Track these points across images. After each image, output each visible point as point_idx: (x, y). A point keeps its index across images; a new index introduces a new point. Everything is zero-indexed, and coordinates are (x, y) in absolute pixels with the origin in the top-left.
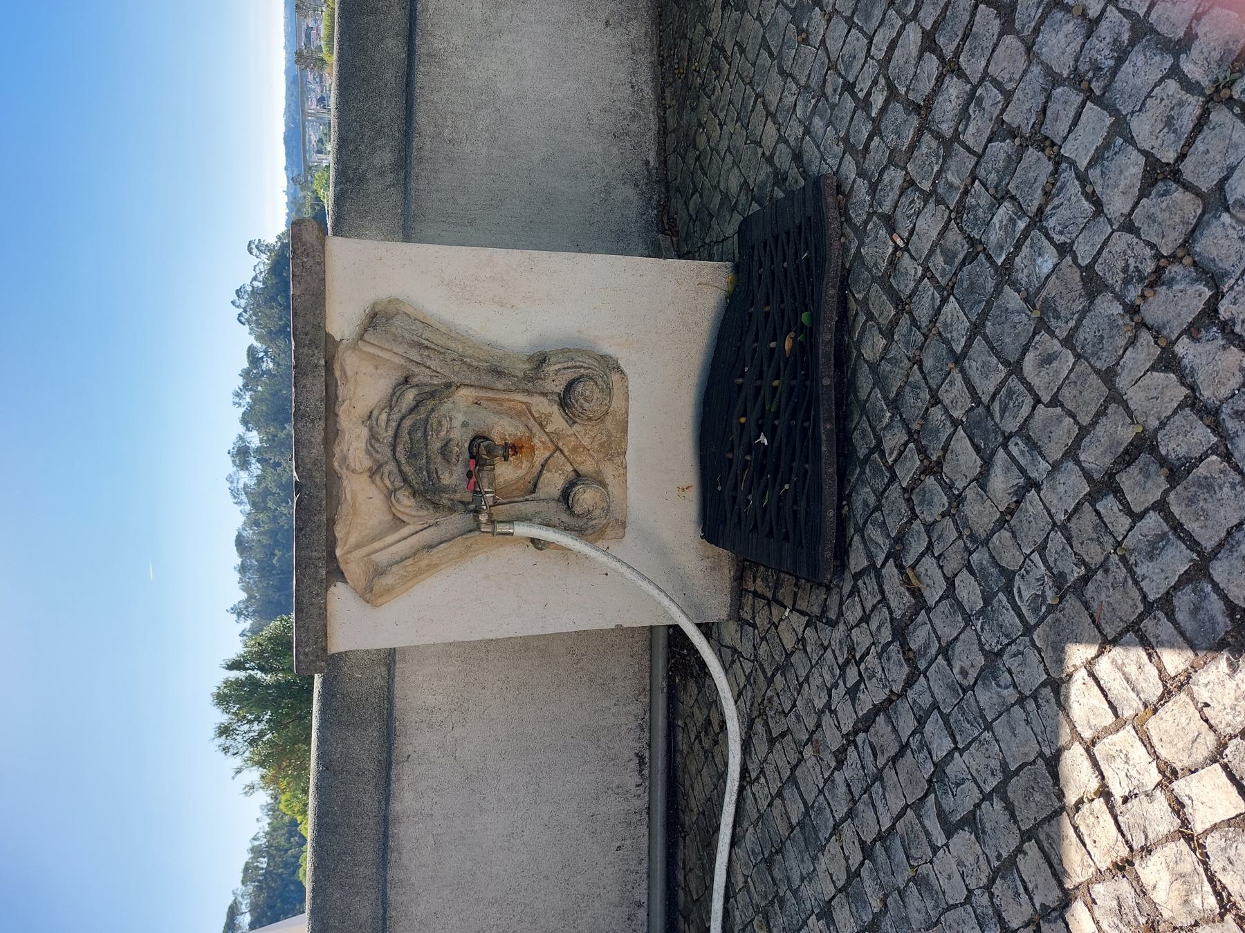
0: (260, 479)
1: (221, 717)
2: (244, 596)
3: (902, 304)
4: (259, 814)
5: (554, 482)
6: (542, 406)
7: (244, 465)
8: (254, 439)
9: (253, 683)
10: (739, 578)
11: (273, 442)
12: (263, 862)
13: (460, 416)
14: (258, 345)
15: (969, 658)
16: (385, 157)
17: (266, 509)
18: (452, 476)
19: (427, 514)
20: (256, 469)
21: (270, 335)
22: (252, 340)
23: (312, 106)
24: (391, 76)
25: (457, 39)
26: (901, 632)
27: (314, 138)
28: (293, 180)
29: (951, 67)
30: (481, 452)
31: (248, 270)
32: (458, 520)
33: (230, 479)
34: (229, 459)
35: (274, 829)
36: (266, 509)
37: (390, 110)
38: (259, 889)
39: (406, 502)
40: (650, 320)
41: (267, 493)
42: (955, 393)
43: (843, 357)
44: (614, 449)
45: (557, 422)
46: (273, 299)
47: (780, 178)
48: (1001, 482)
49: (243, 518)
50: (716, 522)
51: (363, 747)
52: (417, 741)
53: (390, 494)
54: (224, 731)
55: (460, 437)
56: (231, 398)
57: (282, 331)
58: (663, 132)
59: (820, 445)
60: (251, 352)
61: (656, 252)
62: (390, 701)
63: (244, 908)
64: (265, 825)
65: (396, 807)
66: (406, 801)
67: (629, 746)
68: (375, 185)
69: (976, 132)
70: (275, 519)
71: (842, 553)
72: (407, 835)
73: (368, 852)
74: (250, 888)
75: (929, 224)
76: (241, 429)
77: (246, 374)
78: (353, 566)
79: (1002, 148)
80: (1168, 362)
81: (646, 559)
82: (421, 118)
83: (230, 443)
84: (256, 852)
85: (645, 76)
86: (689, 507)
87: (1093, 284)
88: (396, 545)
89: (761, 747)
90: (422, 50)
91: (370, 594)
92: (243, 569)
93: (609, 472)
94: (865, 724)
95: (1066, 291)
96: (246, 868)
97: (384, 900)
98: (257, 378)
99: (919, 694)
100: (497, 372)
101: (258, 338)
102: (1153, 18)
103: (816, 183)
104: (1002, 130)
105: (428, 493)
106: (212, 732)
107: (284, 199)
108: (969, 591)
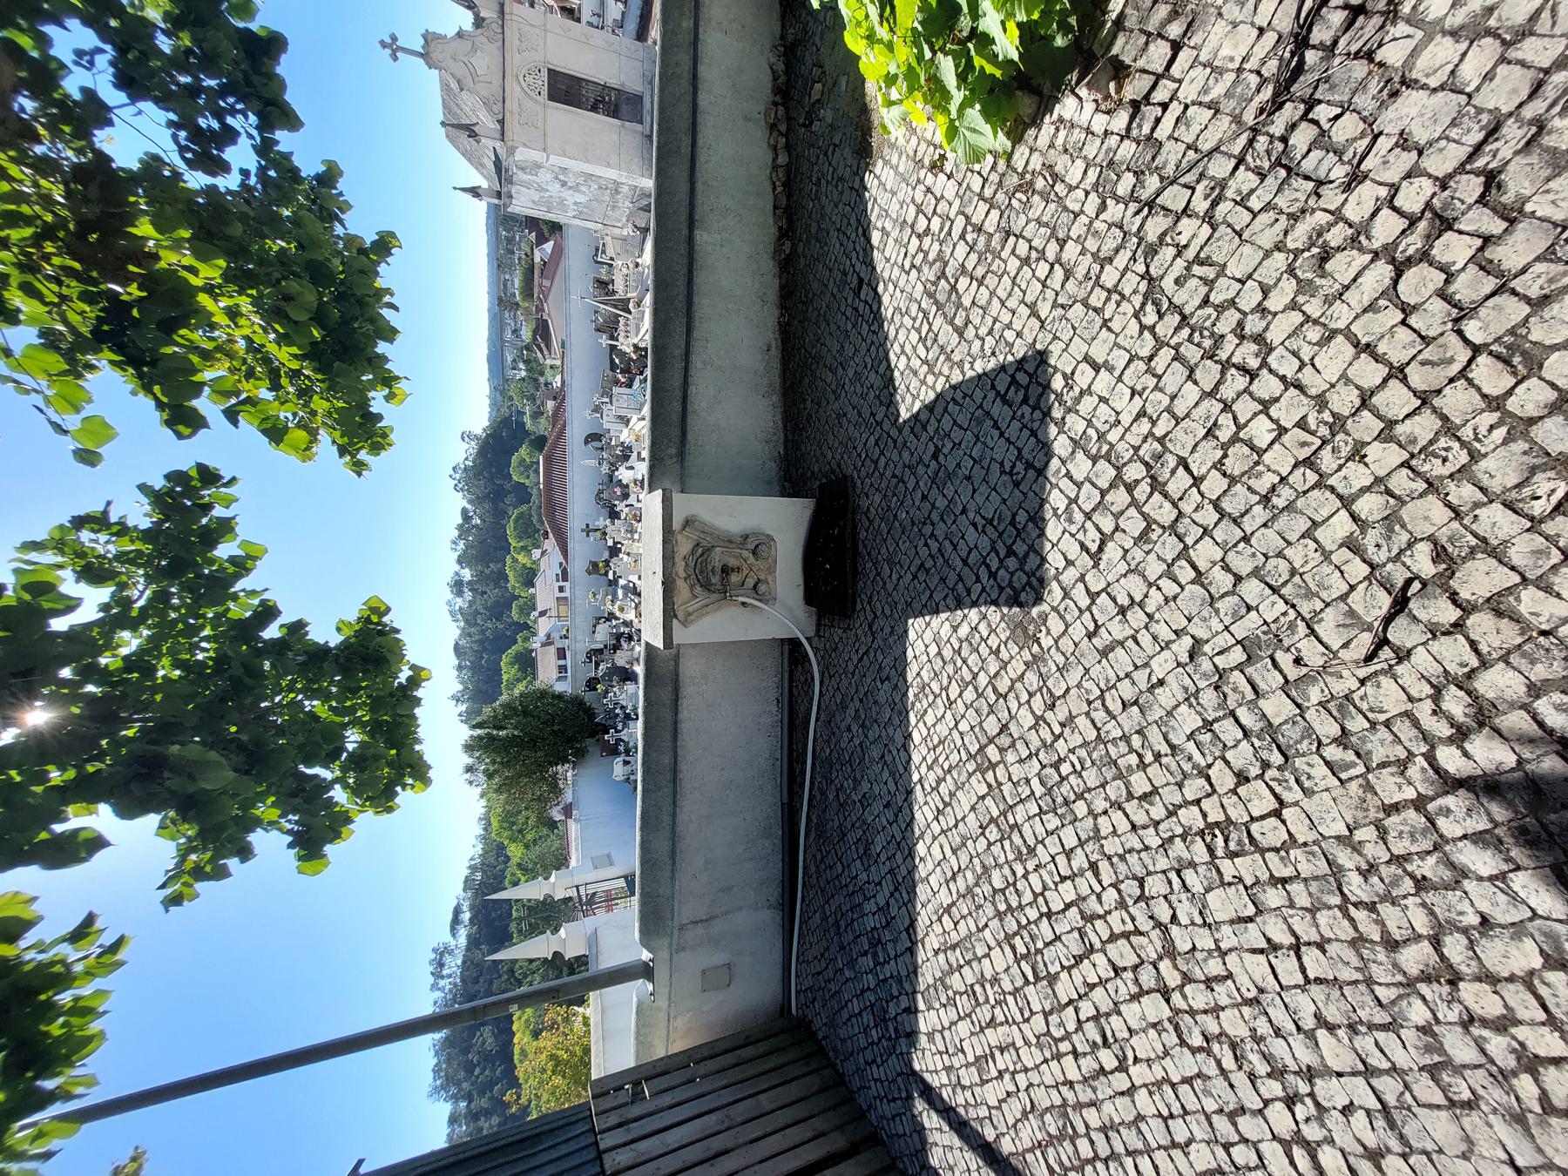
0: (471, 603)
1: (467, 760)
2: (461, 687)
3: (871, 522)
4: (474, 842)
5: (750, 582)
6: (746, 554)
7: (460, 593)
8: (467, 574)
9: (491, 738)
10: (819, 620)
11: (480, 577)
12: (478, 876)
13: (718, 558)
14: (469, 507)
15: (887, 630)
16: (673, 451)
17: (476, 624)
18: (715, 580)
19: (706, 594)
20: (468, 595)
21: (477, 501)
22: (465, 504)
23: (509, 335)
24: (675, 418)
25: (704, 404)
26: (870, 627)
27: (509, 359)
28: (495, 389)
29: (882, 453)
30: (726, 570)
31: (461, 453)
32: (716, 596)
33: (449, 603)
34: (448, 589)
35: (485, 853)
36: (476, 624)
37: (675, 432)
38: (476, 894)
39: (698, 589)
40: (782, 521)
41: (477, 613)
42: (884, 551)
43: (855, 536)
44: (772, 570)
45: (752, 559)
46: (480, 473)
47: (833, 472)
48: (894, 577)
49: (458, 632)
50: (810, 597)
51: (665, 695)
52: (688, 690)
53: (692, 587)
54: (469, 769)
55: (718, 566)
56: (449, 545)
57: (487, 496)
58: (786, 441)
59: (21, 214)
60: (464, 512)
61: (784, 493)
62: (677, 675)
63: (465, 908)
64: (479, 849)
65: (680, 716)
66: (684, 714)
67: (773, 695)
68: (668, 462)
69: (888, 473)
70: (483, 632)
71: (854, 605)
72: (685, 727)
73: (668, 736)
74: (469, 894)
75: (877, 498)
76: (457, 567)
77: (460, 527)
78: (680, 614)
79: (894, 480)
80: (926, 545)
81: (783, 613)
82: (689, 437)
83: (448, 577)
84: (473, 868)
85: (779, 418)
86: (800, 592)
87: (913, 523)
88: (694, 605)
89: (826, 682)
90: (690, 409)
91: (685, 624)
92: (460, 668)
93: (770, 579)
94: (860, 660)
95: (907, 523)
96: (467, 880)
97: (675, 754)
98: (468, 531)
99: (875, 645)
100: (730, 541)
101: (469, 502)
102: (425, 1003)
103: (845, 476)
104: (894, 476)
105: (707, 586)
106: (461, 770)
107: (487, 401)
108: (887, 612)
